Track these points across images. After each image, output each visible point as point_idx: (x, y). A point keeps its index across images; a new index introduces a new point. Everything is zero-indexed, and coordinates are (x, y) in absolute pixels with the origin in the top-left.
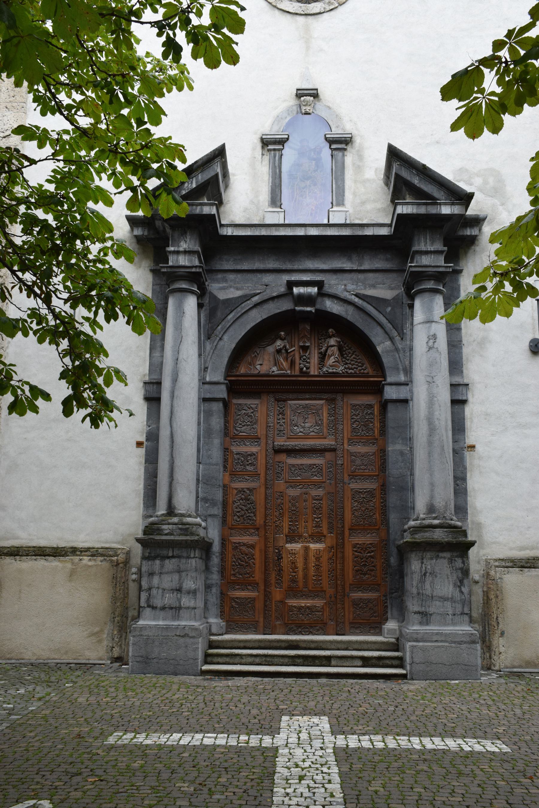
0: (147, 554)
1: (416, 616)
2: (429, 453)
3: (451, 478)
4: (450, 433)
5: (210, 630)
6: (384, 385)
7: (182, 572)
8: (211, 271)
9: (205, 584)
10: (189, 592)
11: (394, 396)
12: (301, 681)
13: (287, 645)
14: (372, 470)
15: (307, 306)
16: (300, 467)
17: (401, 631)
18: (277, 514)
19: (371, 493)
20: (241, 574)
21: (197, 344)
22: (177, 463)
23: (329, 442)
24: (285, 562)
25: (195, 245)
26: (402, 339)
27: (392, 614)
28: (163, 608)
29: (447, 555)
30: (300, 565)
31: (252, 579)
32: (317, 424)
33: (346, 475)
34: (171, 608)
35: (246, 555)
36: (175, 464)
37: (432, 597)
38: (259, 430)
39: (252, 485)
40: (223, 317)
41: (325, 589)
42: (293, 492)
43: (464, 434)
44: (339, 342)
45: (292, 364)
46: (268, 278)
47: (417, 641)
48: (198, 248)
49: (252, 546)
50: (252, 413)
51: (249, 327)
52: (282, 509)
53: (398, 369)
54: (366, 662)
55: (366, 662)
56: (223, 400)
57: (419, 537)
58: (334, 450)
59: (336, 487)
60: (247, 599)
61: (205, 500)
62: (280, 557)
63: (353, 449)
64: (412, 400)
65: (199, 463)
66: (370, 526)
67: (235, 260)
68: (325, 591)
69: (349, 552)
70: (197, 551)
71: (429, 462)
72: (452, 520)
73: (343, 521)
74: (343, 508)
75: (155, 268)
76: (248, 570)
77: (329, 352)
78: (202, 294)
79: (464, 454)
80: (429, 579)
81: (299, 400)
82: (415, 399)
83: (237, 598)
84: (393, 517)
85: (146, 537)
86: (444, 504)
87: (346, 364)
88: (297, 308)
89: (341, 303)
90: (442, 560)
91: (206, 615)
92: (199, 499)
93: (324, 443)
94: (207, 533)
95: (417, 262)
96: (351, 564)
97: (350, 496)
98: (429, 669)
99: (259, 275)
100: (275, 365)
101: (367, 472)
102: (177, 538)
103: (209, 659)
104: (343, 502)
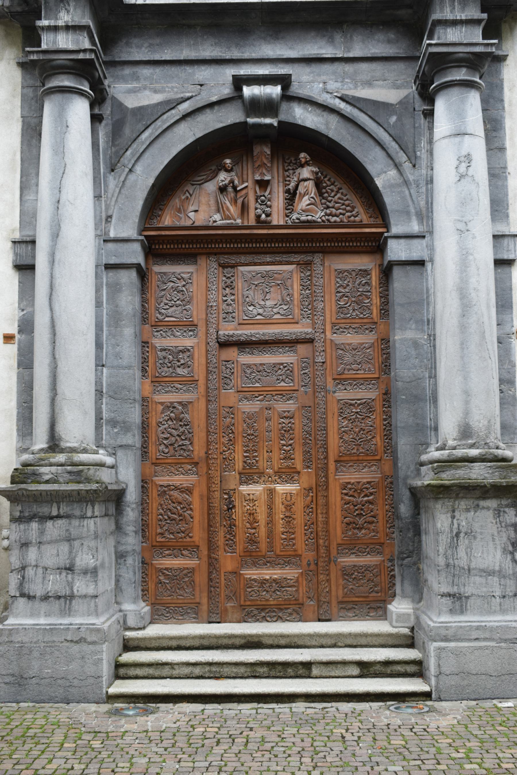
0: (18, 514)
1: (444, 600)
2: (462, 344)
3: (496, 382)
4: (494, 310)
5: (125, 622)
6: (386, 238)
7: (74, 540)
8: (113, 64)
9: (116, 552)
10: (85, 572)
11: (403, 256)
12: (266, 708)
13: (243, 641)
14: (370, 370)
15: (265, 116)
16: (260, 369)
17: (417, 618)
18: (225, 440)
19: (368, 405)
20: (172, 533)
21: (90, 177)
22: (62, 367)
23: (302, 329)
24: (239, 514)
25: (83, 17)
26: (414, 166)
27: (402, 590)
28: (46, 598)
29: (492, 503)
30: (262, 517)
31: (188, 539)
32: (284, 302)
33: (329, 379)
34: (59, 597)
35: (180, 503)
36: (59, 370)
37: (469, 570)
38: (195, 313)
39: (185, 397)
40: (135, 136)
41: (300, 552)
42: (249, 407)
43: (512, 313)
44: (317, 173)
45: (244, 209)
46: (203, 73)
47: (446, 639)
48: (87, 21)
49: (189, 491)
50: (184, 286)
51: (174, 152)
52: (233, 432)
53: (408, 213)
54: (366, 669)
55: (366, 669)
56: (138, 267)
57: (448, 477)
58: (311, 341)
59: (315, 397)
60: (181, 570)
61: (113, 423)
62: (231, 507)
63: (340, 339)
64: (432, 260)
65: (100, 364)
66: (367, 455)
67: (151, 45)
68: (300, 556)
69: (336, 497)
70: (96, 507)
71: (462, 357)
72: (497, 448)
73: (327, 448)
74: (326, 429)
75: (24, 60)
76: (183, 526)
77: (301, 189)
78: (98, 98)
79: (510, 343)
80: (463, 542)
81: (255, 264)
82: (437, 258)
83: (166, 569)
84: (403, 443)
85: (15, 487)
86: (486, 423)
87: (328, 207)
88: (251, 120)
89: (319, 111)
90: (484, 512)
91: (119, 599)
92: (104, 421)
93: (296, 330)
94: (116, 473)
95: (439, 38)
96: (339, 513)
97: (336, 410)
98: (465, 682)
99: (189, 69)
100: (218, 211)
101: (361, 374)
102: (64, 487)
103: (122, 671)
104: (325, 420)
